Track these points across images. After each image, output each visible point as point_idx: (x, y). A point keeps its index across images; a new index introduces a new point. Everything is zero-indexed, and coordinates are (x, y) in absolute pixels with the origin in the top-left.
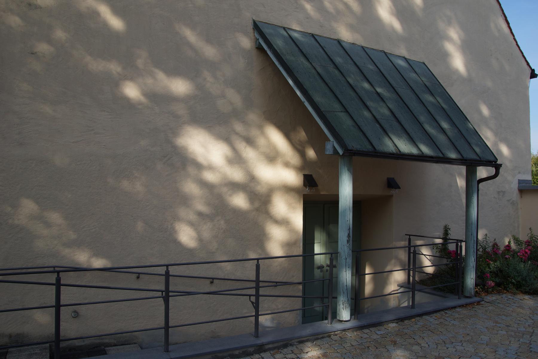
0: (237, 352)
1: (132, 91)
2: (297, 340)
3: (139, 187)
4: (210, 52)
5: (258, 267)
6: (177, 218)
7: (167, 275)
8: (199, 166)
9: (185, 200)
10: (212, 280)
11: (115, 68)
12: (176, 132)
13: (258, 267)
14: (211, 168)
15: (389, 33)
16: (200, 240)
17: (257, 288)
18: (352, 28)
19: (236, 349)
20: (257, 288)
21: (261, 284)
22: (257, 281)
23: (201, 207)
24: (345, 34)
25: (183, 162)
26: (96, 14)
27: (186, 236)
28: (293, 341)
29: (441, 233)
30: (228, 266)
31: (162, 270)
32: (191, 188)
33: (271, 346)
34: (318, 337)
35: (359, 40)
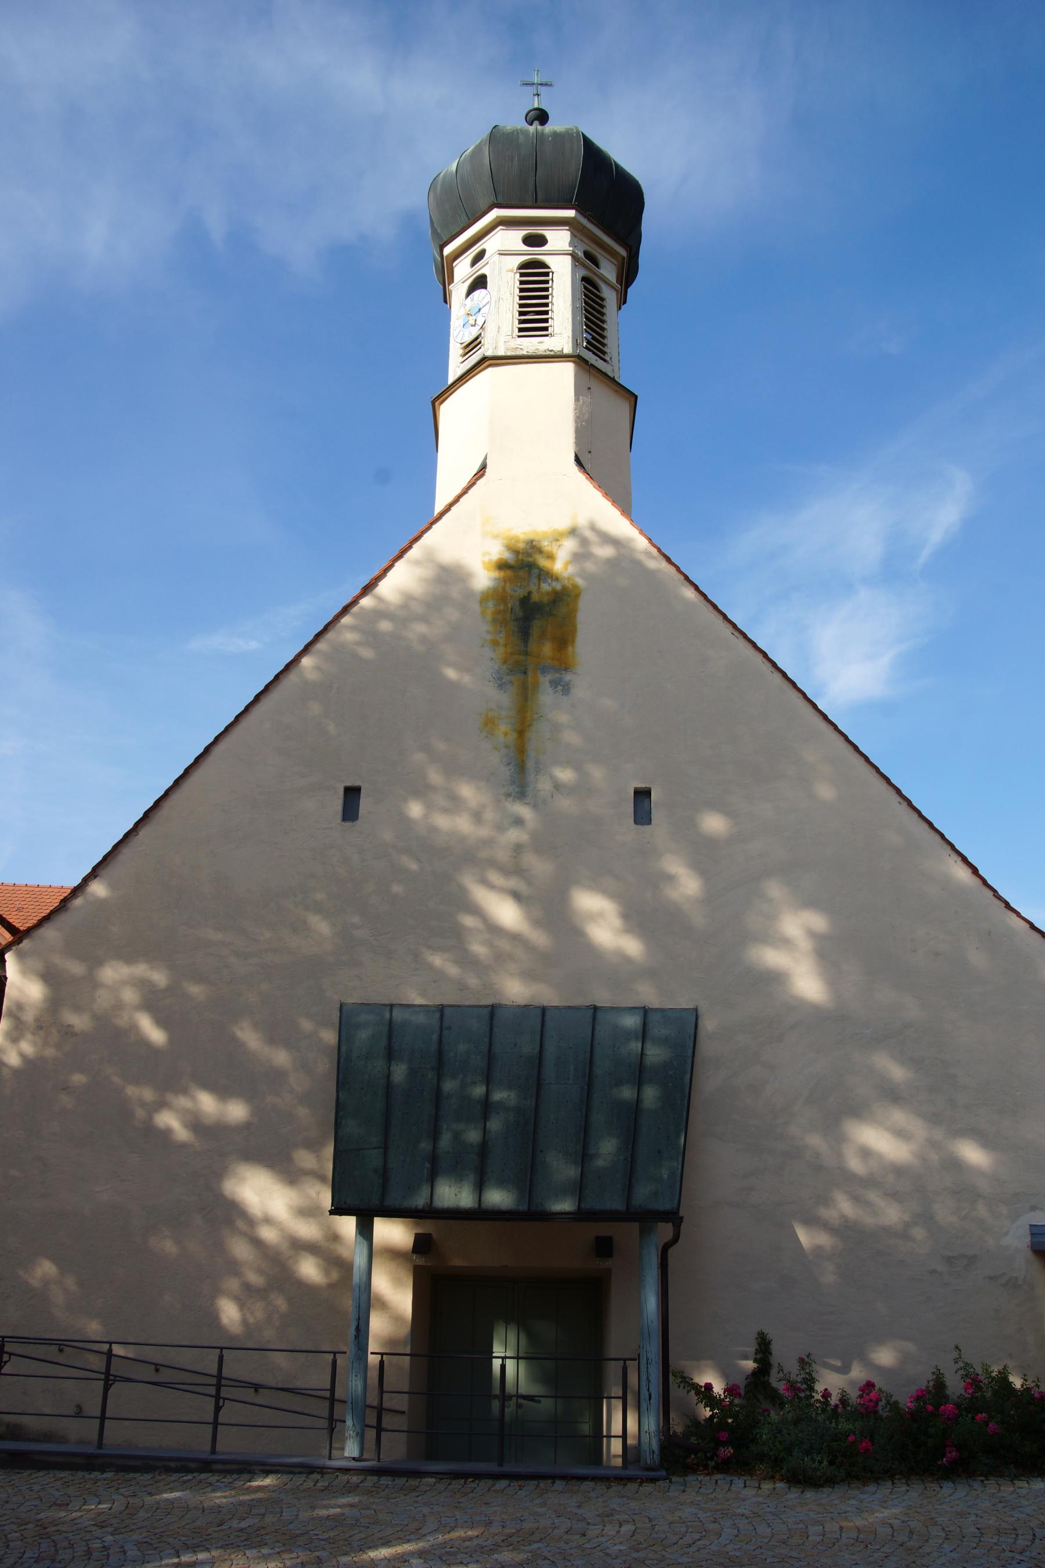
0: (173, 1464)
1: (169, 1120)
2: (260, 1468)
3: (169, 1247)
4: (281, 1058)
5: (221, 1358)
6: (217, 1292)
7: (110, 1354)
8: (251, 1222)
9: (233, 1267)
10: (157, 1367)
11: (148, 1094)
12: (219, 1173)
13: (221, 1358)
14: (268, 1220)
15: (617, 970)
16: (245, 1322)
17: (219, 1387)
18: (529, 975)
19: (171, 1459)
20: (219, 1387)
21: (223, 1382)
22: (219, 1376)
23: (254, 1278)
24: (515, 990)
25: (232, 1214)
26: (134, 1028)
27: (230, 1313)
28: (254, 1467)
29: (751, 1349)
30: (281, 1360)
31: (106, 1347)
32: (241, 1250)
33: (220, 1467)
34: (292, 1469)
35: (546, 995)
